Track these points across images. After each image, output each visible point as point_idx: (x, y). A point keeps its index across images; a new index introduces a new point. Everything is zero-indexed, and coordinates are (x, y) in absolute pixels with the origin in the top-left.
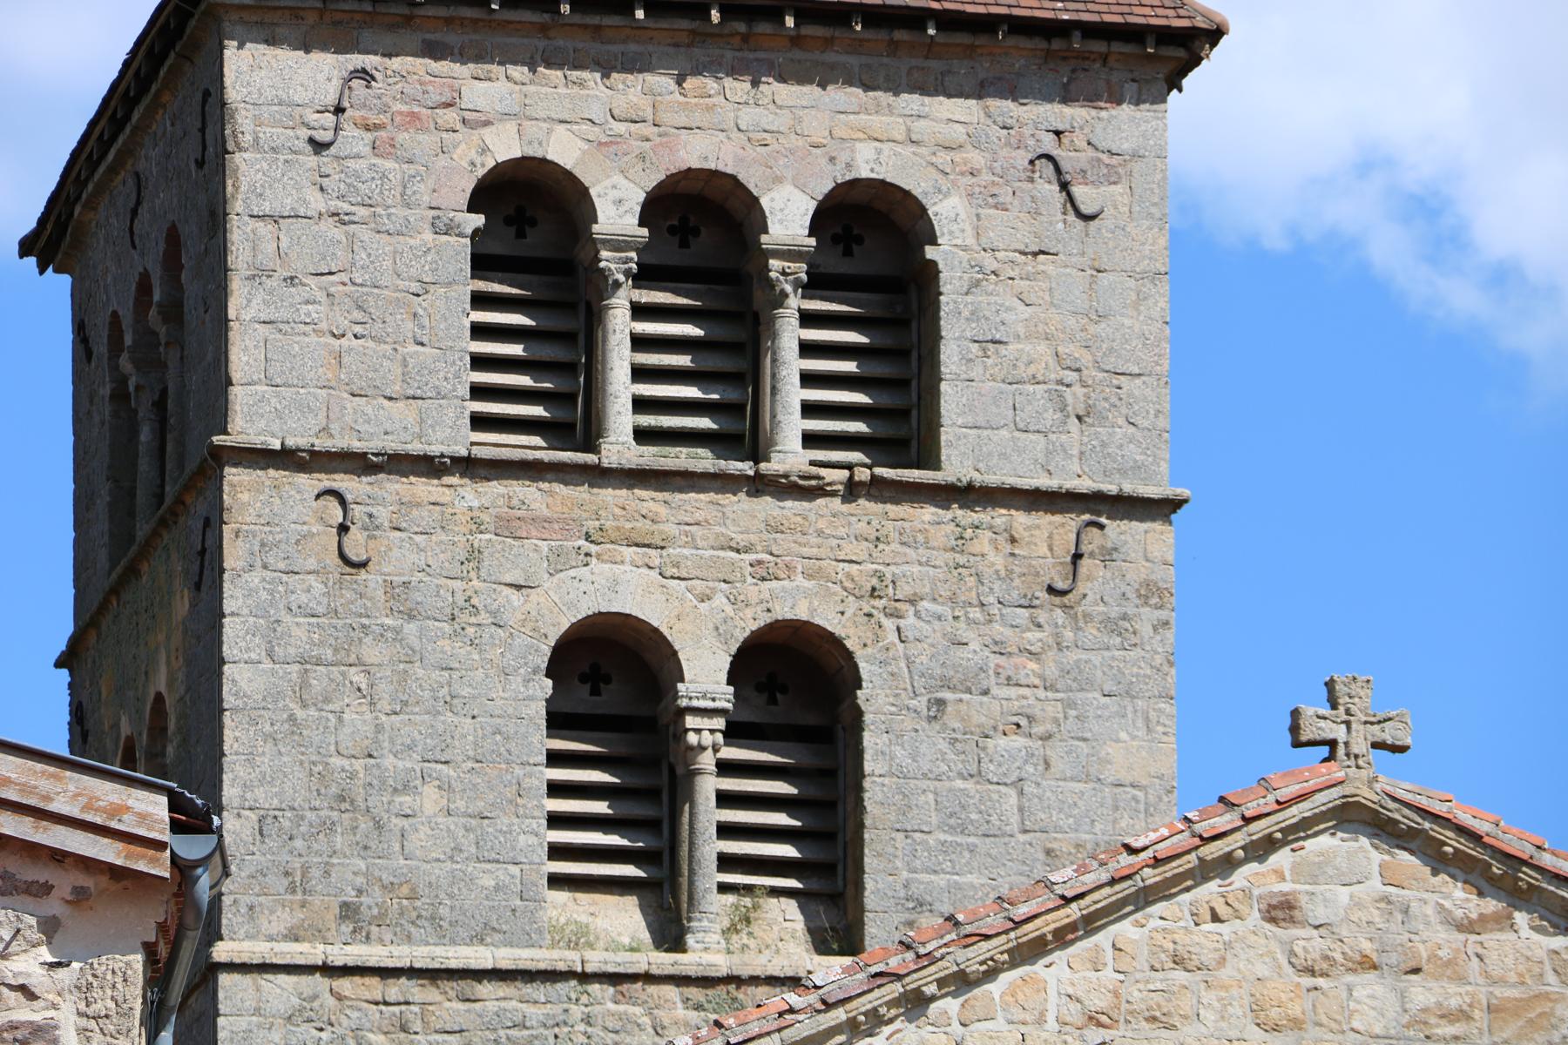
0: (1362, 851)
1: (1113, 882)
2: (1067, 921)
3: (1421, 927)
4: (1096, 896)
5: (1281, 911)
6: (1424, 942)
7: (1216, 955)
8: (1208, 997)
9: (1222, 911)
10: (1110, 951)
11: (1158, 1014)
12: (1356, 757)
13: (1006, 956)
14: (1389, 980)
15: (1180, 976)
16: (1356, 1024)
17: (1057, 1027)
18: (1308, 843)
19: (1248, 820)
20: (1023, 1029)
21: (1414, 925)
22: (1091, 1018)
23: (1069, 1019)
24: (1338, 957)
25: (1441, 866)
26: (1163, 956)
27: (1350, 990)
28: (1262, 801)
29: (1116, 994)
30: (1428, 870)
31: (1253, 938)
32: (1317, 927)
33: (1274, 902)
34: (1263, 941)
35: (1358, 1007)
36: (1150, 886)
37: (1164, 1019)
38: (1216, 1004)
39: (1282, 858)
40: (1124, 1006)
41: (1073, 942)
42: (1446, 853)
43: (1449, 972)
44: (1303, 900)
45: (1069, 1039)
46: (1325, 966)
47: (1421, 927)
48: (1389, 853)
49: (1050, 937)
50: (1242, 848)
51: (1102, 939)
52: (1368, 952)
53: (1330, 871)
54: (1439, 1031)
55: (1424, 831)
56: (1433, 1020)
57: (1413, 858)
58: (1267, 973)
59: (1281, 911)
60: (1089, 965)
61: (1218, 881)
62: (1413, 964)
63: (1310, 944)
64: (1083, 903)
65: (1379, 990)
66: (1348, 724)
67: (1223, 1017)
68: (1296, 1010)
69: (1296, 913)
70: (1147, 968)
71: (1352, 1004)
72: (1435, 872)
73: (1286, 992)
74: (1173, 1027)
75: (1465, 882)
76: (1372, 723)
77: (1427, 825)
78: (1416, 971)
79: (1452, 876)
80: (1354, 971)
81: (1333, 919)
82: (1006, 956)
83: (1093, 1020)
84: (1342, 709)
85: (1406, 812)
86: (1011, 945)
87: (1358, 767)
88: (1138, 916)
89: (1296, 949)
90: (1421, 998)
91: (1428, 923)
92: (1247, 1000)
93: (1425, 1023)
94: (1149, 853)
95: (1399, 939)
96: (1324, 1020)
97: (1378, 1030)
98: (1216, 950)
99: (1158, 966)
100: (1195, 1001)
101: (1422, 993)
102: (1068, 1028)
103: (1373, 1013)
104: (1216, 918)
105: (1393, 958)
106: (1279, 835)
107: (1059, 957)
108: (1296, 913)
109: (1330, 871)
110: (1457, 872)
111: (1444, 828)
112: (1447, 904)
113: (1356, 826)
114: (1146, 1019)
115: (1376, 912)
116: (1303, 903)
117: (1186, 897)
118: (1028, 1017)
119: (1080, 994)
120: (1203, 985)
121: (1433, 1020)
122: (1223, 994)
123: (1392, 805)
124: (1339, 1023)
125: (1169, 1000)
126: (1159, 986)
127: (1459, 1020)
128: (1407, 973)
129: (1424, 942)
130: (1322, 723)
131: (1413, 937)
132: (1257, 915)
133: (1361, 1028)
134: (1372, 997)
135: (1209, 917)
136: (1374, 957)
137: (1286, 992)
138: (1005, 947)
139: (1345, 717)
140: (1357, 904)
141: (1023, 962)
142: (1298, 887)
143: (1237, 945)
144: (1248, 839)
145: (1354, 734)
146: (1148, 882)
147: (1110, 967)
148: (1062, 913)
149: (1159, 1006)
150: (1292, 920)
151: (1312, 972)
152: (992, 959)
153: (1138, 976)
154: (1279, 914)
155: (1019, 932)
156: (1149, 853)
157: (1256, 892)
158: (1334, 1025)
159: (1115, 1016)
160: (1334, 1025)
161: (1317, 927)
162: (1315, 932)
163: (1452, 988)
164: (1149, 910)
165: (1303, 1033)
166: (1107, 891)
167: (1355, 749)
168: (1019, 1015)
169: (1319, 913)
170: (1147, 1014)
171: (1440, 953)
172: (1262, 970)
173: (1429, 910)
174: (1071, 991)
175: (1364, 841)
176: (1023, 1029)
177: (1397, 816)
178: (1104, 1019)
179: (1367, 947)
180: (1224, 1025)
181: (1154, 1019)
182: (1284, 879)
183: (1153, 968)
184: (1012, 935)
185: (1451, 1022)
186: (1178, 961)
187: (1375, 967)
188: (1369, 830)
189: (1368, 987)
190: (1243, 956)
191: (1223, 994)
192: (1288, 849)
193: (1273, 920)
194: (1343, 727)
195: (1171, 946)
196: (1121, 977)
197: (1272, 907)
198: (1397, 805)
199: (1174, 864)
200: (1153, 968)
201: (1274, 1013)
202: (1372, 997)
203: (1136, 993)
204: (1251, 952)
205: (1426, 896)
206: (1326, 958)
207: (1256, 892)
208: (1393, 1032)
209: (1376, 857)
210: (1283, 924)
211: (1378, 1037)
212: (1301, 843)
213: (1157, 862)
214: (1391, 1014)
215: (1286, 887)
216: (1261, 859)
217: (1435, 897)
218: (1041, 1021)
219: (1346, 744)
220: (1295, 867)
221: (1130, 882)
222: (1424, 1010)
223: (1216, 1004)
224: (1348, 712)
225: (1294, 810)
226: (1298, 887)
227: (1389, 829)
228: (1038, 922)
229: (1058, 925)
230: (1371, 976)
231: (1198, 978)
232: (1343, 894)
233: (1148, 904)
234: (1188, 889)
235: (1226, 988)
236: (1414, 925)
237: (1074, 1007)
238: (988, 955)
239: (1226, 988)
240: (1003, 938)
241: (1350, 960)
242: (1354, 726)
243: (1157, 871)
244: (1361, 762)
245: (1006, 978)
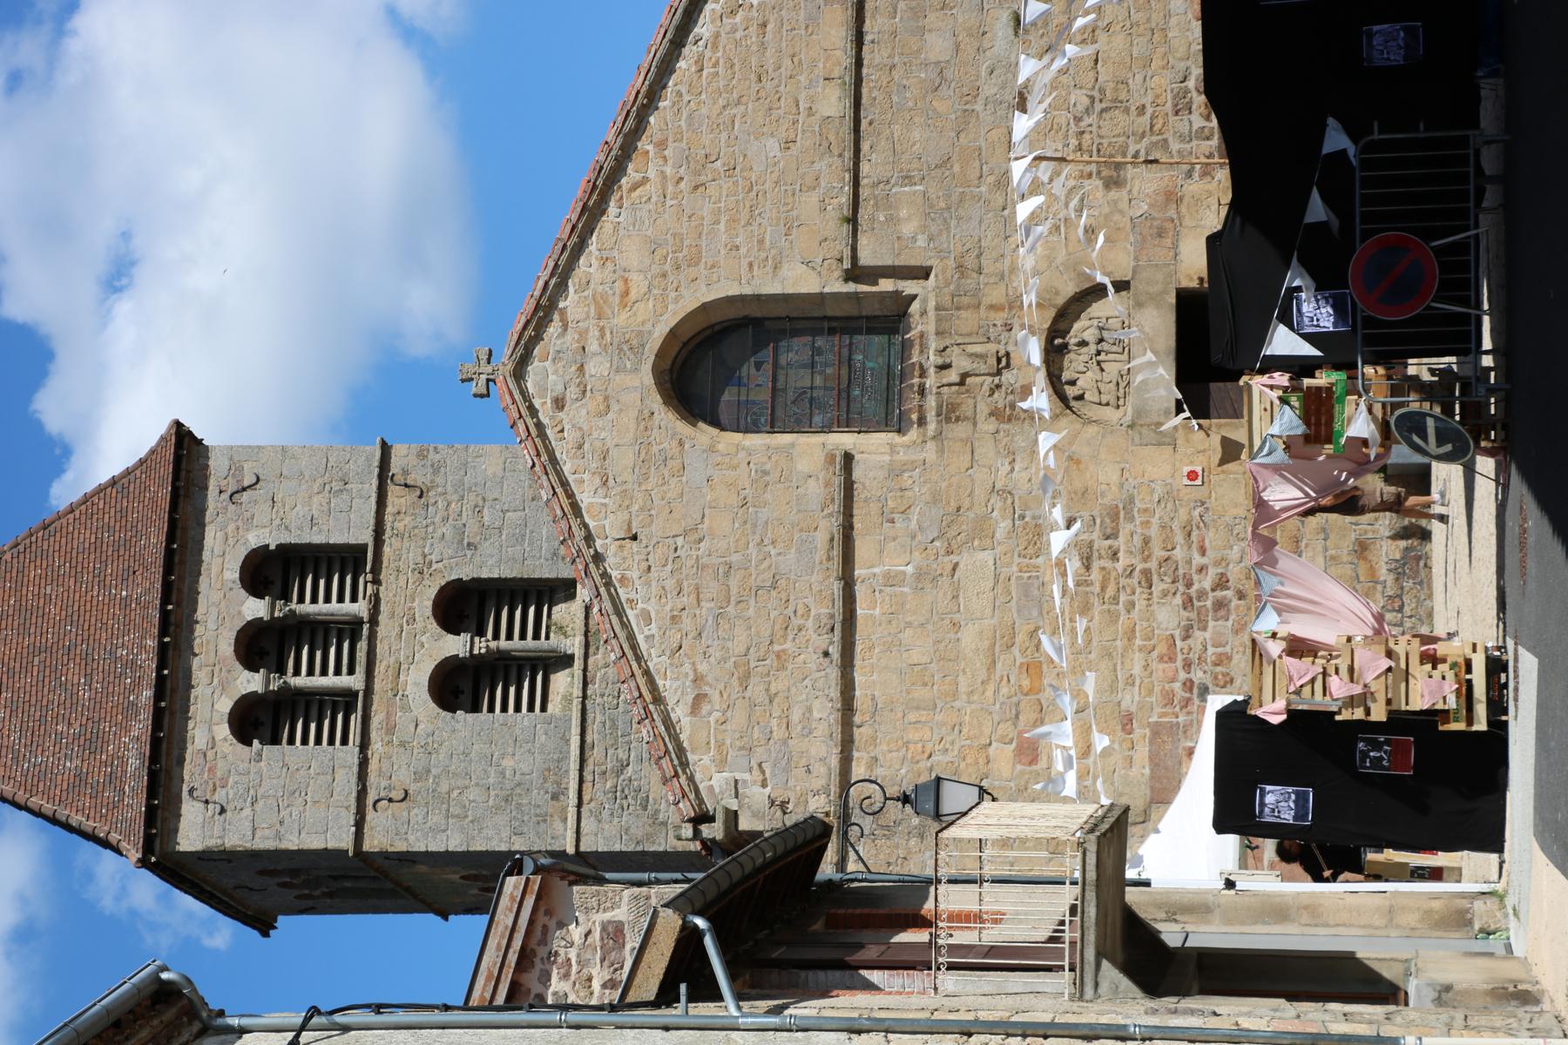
0: (534, 368)
5: (559, 403)
8: (595, 435)
15: (586, 446)
39: (537, 403)
51: (571, 479)
59: (559, 403)
63: (572, 393)
73: (593, 402)
83: (605, 483)
101: (593, 346)
137: (593, 402)
140: (556, 372)
169: (560, 387)
172: (584, 412)
179: (574, 368)
186: (580, 447)
209: (536, 363)
213: (538, 455)
218: (605, 505)
232: (551, 377)
245: (587, 520)
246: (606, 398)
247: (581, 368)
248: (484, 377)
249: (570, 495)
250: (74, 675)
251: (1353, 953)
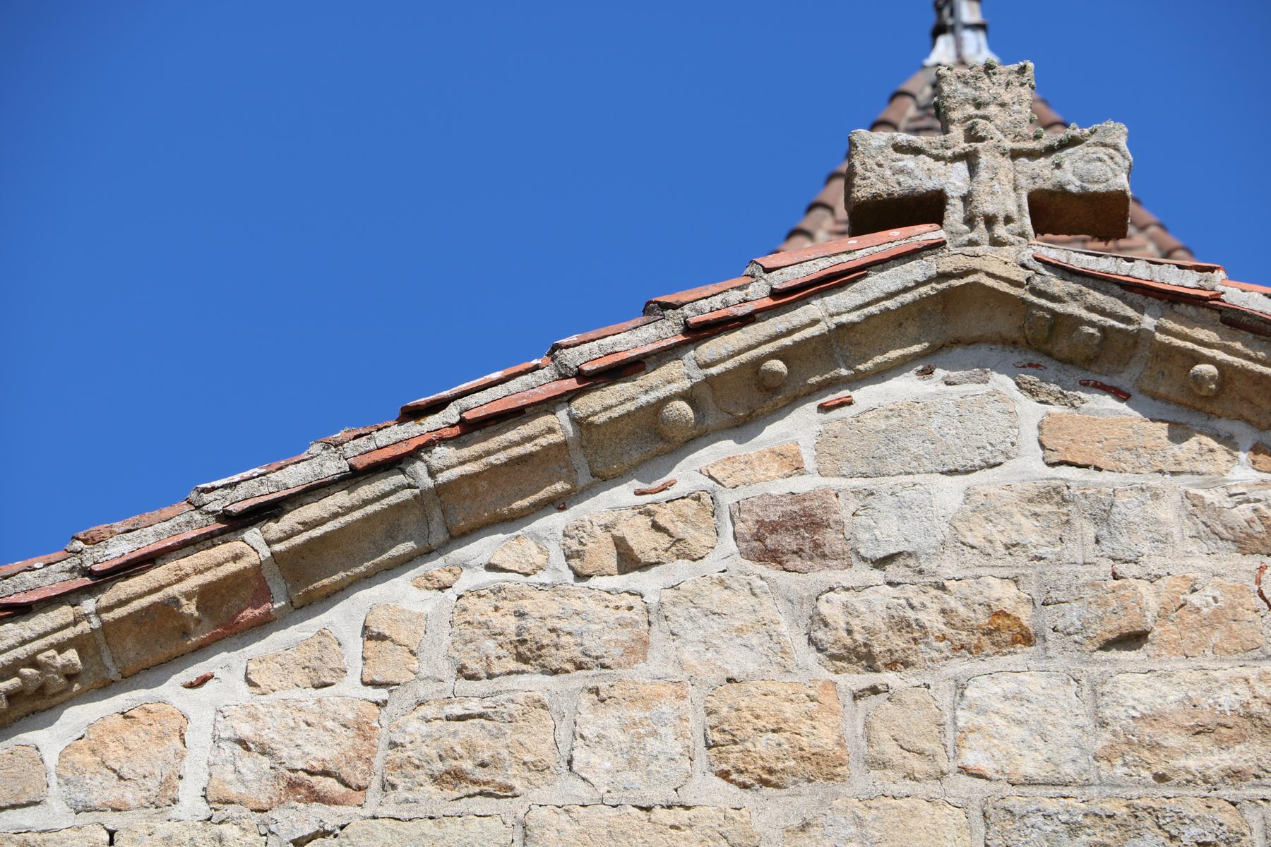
0: (999, 406)
1: (354, 477)
2: (231, 568)
3: (1145, 547)
4: (311, 511)
5: (785, 538)
6: (1153, 579)
7: (625, 635)
8: (593, 721)
9: (643, 542)
10: (355, 645)
11: (467, 765)
12: (990, 221)
13: (72, 655)
14: (1061, 662)
15: (534, 683)
16: (971, 759)
17: (203, 810)
18: (864, 396)
19: (698, 333)
20: (112, 820)
21: (1123, 544)
22: (293, 786)
23: (233, 791)
24: (932, 620)
25: (1197, 420)
26: (490, 646)
27: (960, 688)
28: (735, 296)
29: (362, 729)
30: (1162, 430)
31: (718, 594)
32: (881, 563)
33: (773, 516)
34: (745, 601)
35: (981, 721)
36: (449, 485)
37: (480, 774)
38: (615, 735)
39: (800, 426)
40: (382, 755)
41: (264, 625)
42: (1199, 380)
43: (1216, 637)
44: (845, 508)
45: (229, 831)
46: (899, 642)
47: (1145, 547)
48: (1061, 399)
49: (190, 608)
50: (685, 396)
51: (340, 620)
52: (1007, 605)
53: (914, 446)
54: (1192, 763)
55: (1140, 337)
56: (1174, 740)
57: (1123, 407)
58: (751, 667)
59: (785, 538)
60: (299, 676)
61: (636, 484)
62: (1125, 624)
63: (866, 602)
64: (274, 528)
65: (1034, 683)
66: (971, 159)
67: (632, 763)
68: (824, 737)
69: (830, 538)
70: (447, 671)
71: (963, 717)
72: (1179, 433)
73: (805, 701)
74: (506, 792)
75: (1256, 449)
76: (1032, 155)
77: (1148, 322)
78: (1133, 639)
79: (1229, 442)
80: (974, 650)
81: (917, 542)
82: (72, 655)
83: (301, 786)
84: (957, 132)
85: (1096, 297)
86: (84, 627)
87: (996, 242)
88: (434, 567)
89: (824, 608)
90: (1144, 694)
91: (1165, 539)
92: (696, 724)
93: (1154, 747)
94: (451, 414)
95: (1085, 574)
96: (891, 750)
97: (1029, 766)
98: (622, 624)
99: (474, 666)
100: (564, 734)
101: (1137, 685)
102: (231, 810)
103: (1018, 732)
104: (629, 561)
105: (1072, 615)
106: (778, 365)
107: (226, 665)
108: (830, 538)
109: (914, 446)
110: (1238, 428)
111: (1192, 322)
112: (1213, 496)
113: (983, 351)
114: (435, 779)
115: (1028, 524)
116: (845, 515)
117: (556, 521)
118: (130, 795)
119: (268, 736)
120: (587, 699)
121: (1174, 740)
122: (637, 713)
123: (1057, 285)
124: (932, 757)
125: (499, 735)
126: (475, 706)
127: (1242, 738)
128: (1107, 646)
129: (1153, 579)
130: (909, 161)
131: (1121, 568)
132: (731, 546)
133: (987, 767)
134: (1018, 697)
135: (612, 562)
136: (1025, 615)
137: (805, 701)
138: (69, 633)
139: (962, 146)
140: (985, 510)
141: (131, 677)
142: (835, 482)
143: (679, 614)
144: (698, 375)
145: (983, 175)
146: (442, 478)
147: (353, 678)
148: (221, 551)
149: (471, 748)
150: (820, 553)
151: (864, 657)
152: (32, 662)
153: (423, 690)
154: (788, 541)
155: (105, 599)
156: (451, 414)
157: (728, 499)
158: (915, 763)
159: (356, 778)
160: (915, 763)
161: (881, 563)
162: (877, 576)
163: (1226, 670)
164: (459, 553)
165: (838, 787)
166: (341, 498)
167: (987, 205)
168: (104, 789)
169: (888, 533)
170: (439, 767)
171: (1195, 599)
172: (738, 661)
173: (1167, 512)
174: (246, 730)
175: (1003, 382)
176: (112, 820)
177: (1073, 309)
178: (328, 785)
179: (1005, 595)
180: (633, 777)
181: (458, 776)
182: (799, 470)
183: (463, 673)
184: (88, 605)
185: (1222, 744)
186: (528, 653)
187: (1026, 638)
188: (1016, 357)
189: (1000, 681)
190: (691, 633)
191: (637, 713)
192: (812, 406)
193: (773, 556)
194: (962, 167)
195: (512, 623)
196: (381, 694)
197: (766, 528)
198: (1073, 287)
199: (513, 435)
200: (463, 673)
201: (764, 746)
202: (1018, 697)
203: (414, 726)
204: (715, 625)
205: (1156, 481)
206: (902, 625)
207: (728, 499)
208: (1068, 770)
209: (1030, 411)
210: (795, 562)
211: (1030, 782)
212: (843, 394)
213: (471, 428)
214: (1065, 732)
215: (800, 485)
216: (744, 424)
217: (1183, 483)
218: (163, 800)
219: (967, 199)
220: (824, 441)
221: (398, 479)
222: (1153, 718)
223: (615, 735)
224: (972, 135)
225: (815, 308)
226: (835, 482)
227: (1063, 346)
228: (158, 574)
229: (209, 577)
230: (1022, 656)
231: (579, 684)
232: (950, 492)
233: (459, 536)
234: (558, 503)
235: (644, 701)
236: (1123, 544)
237: (252, 765)
238: (21, 652)
239: (644, 701)
240: (64, 613)
241: (965, 625)
242: (984, 159)
243: (465, 452)
244: (1001, 230)
245: (76, 717)
246: (823, 767)
247: (1006, 634)
248: (954, 179)
249: (232, 614)
250: (652, 744)
251: (740, 443)
